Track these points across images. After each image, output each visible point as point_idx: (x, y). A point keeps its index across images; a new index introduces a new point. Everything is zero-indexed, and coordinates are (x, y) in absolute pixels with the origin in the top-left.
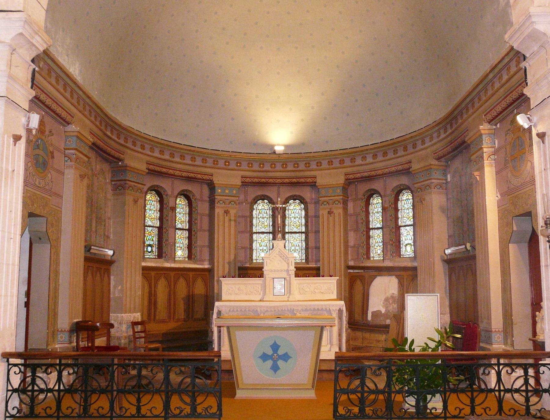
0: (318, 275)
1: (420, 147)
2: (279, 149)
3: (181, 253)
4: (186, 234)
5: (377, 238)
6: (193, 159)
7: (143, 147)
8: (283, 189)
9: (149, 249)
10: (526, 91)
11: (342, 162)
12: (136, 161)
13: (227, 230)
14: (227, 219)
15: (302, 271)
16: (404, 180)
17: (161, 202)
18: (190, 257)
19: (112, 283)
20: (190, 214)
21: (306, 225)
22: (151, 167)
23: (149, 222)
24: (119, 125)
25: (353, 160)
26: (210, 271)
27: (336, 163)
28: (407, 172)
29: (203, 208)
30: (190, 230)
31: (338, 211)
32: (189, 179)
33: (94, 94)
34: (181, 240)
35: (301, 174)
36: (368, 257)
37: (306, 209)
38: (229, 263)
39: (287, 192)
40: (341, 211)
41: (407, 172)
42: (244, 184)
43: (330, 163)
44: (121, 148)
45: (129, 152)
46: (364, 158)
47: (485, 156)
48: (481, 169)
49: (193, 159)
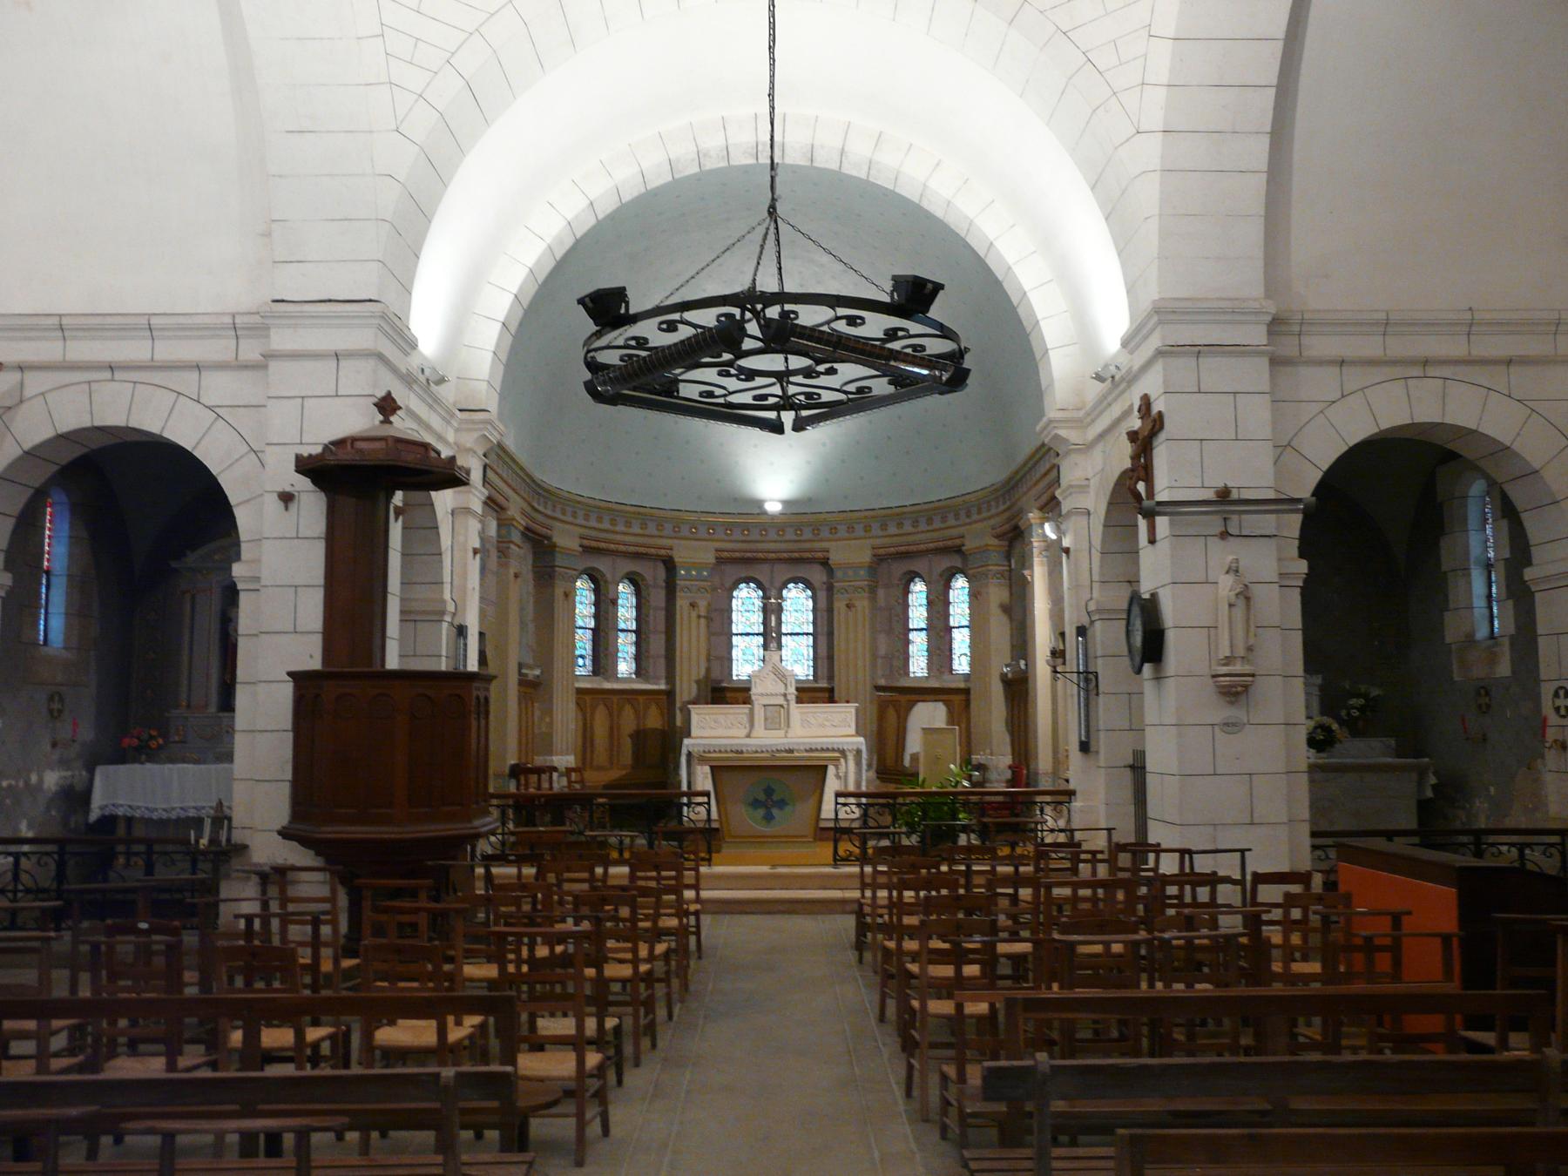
0: (832, 700)
1: (975, 517)
2: (773, 507)
3: (625, 667)
4: (633, 637)
5: (919, 645)
6: (644, 526)
7: (574, 514)
8: (778, 567)
9: (580, 661)
10: (1057, 493)
11: (867, 528)
12: (566, 539)
13: (694, 633)
14: (694, 614)
15: (806, 694)
16: (957, 561)
17: (597, 591)
18: (638, 673)
19: (537, 713)
20: (638, 607)
21: (814, 623)
22: (586, 542)
23: (580, 622)
24: (547, 491)
25: (884, 527)
26: (670, 694)
27: (859, 531)
28: (958, 550)
29: (658, 598)
30: (637, 632)
31: (863, 604)
32: (637, 556)
33: (523, 458)
34: (626, 646)
35: (807, 546)
36: (907, 673)
37: (814, 598)
38: (698, 682)
39: (783, 572)
40: (866, 603)
41: (958, 550)
42: (720, 561)
43: (851, 529)
44: (549, 522)
45: (558, 524)
46: (900, 525)
47: (1036, 551)
48: (1031, 567)
49: (644, 526)
